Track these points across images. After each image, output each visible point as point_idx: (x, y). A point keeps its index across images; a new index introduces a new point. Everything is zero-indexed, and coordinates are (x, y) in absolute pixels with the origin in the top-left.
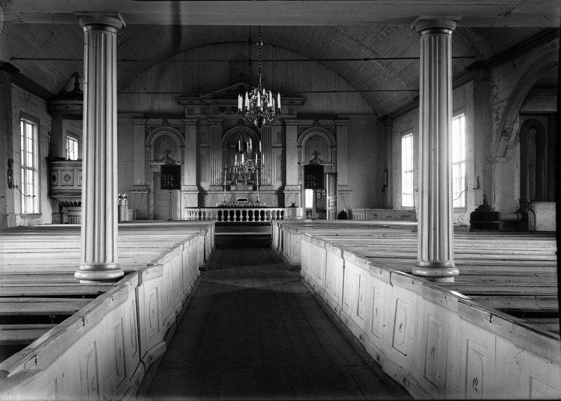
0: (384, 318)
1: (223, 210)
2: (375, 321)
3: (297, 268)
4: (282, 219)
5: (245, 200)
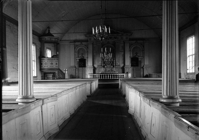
0: (148, 120)
1: (102, 75)
2: (145, 120)
3: (125, 96)
4: (123, 77)
5: (110, 71)
